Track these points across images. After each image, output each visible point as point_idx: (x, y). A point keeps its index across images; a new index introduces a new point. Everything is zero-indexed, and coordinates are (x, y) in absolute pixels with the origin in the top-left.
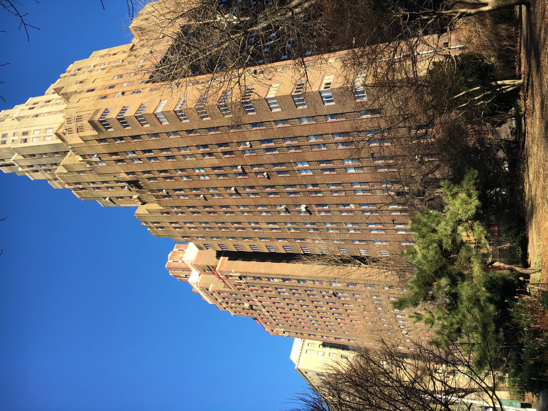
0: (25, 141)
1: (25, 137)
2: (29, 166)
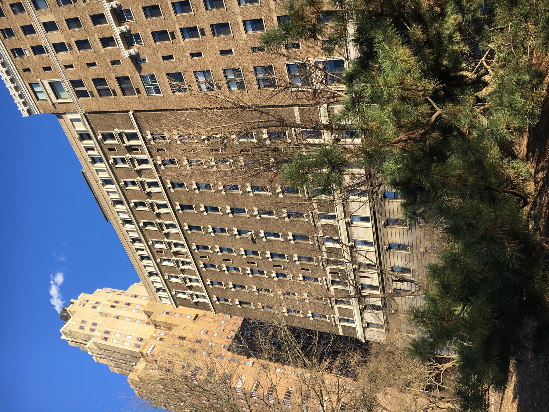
0: (106, 339)
1: (106, 336)
2: (99, 354)
